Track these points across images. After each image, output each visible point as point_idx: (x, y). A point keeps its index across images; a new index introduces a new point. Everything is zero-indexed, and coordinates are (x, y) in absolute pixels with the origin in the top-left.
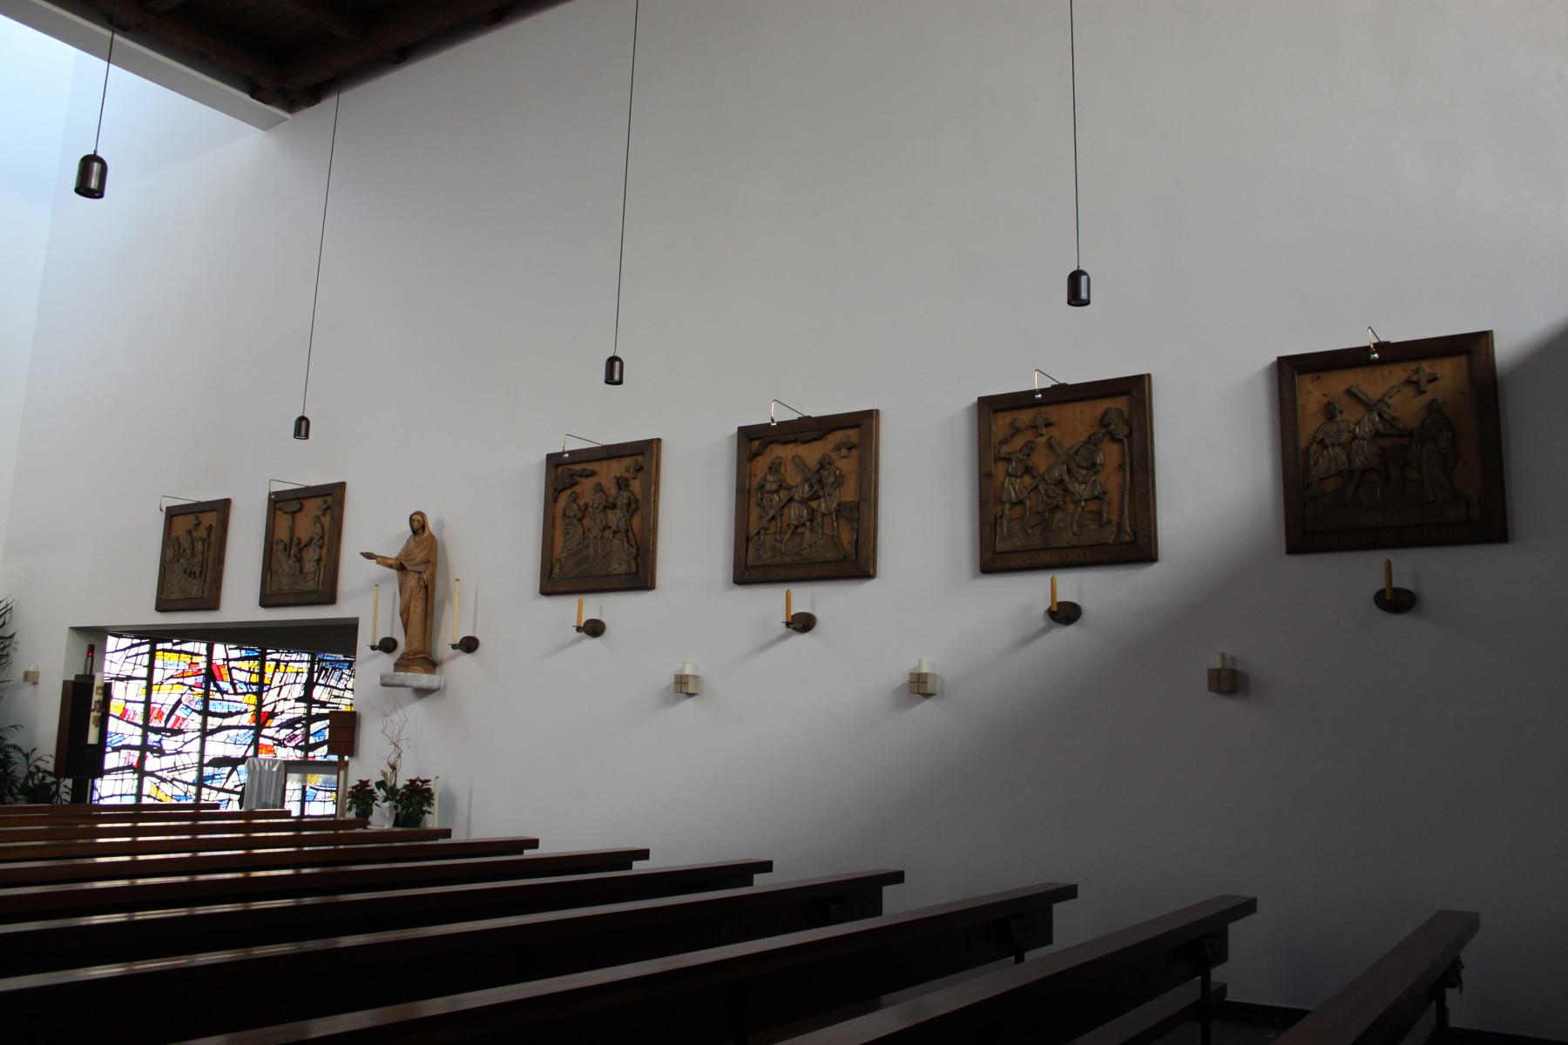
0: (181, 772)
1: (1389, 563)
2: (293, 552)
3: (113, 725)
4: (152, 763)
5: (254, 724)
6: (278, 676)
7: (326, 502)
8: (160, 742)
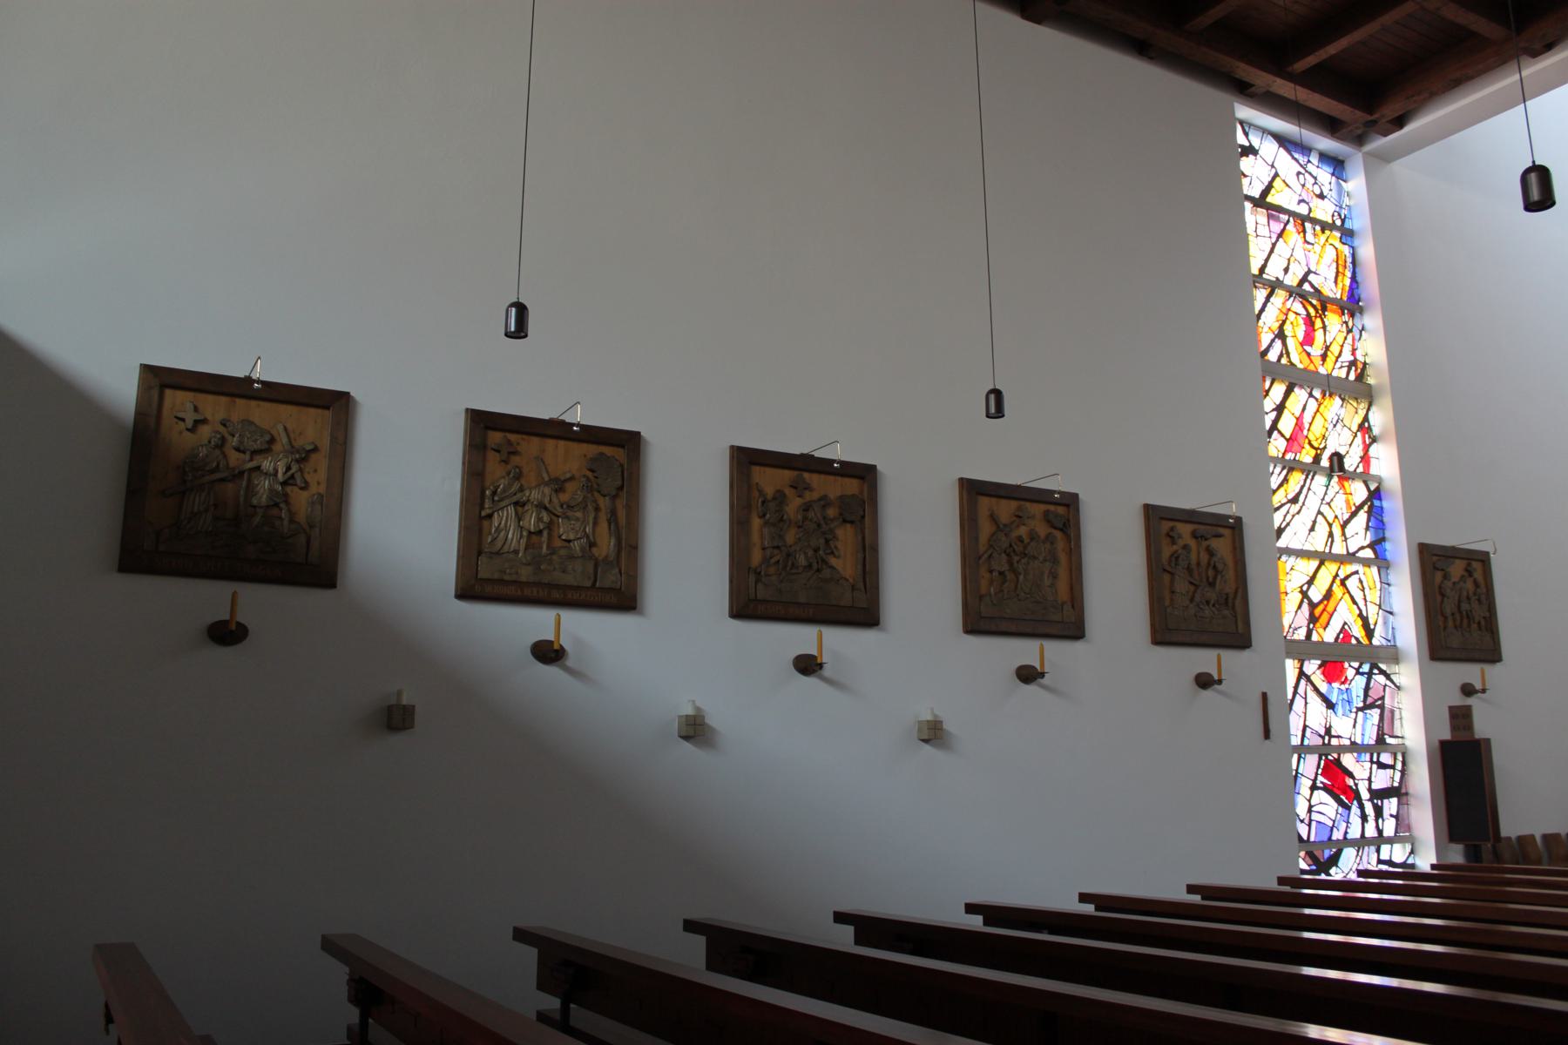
1: (234, 595)
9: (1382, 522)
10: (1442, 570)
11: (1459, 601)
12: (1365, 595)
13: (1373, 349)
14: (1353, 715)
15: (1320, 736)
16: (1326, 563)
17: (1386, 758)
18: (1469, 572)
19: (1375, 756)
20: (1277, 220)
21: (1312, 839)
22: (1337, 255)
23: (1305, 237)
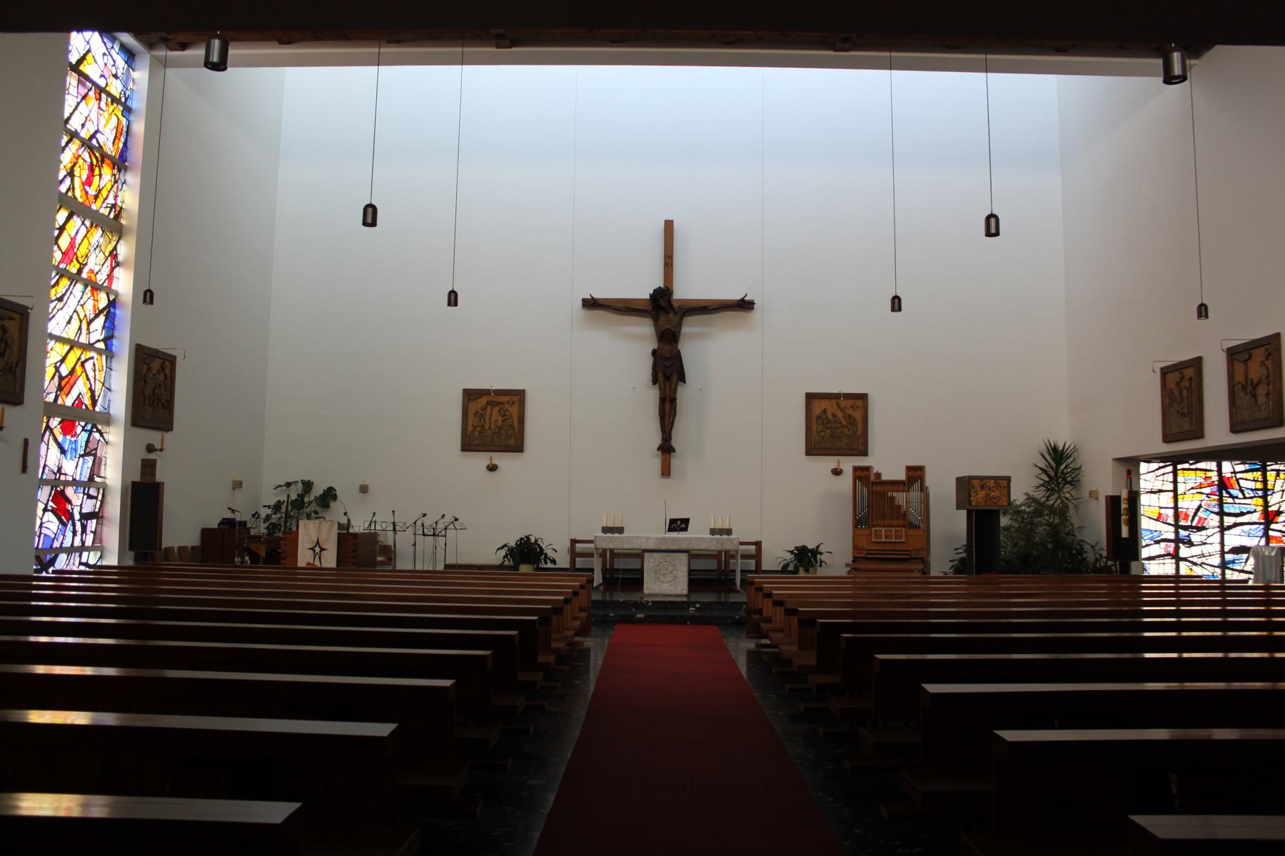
0: (1207, 558)
2: (1248, 390)
3: (1145, 523)
4: (1184, 551)
5: (1262, 521)
6: (1279, 483)
7: (1267, 350)
8: (1188, 536)
9: (113, 324)
10: (148, 364)
11: (155, 387)
12: (95, 375)
13: (130, 199)
14: (77, 459)
15: (54, 473)
16: (75, 349)
17: (93, 492)
18: (163, 368)
19: (87, 489)
20: (84, 85)
21: (40, 546)
22: (118, 124)
23: (99, 104)
